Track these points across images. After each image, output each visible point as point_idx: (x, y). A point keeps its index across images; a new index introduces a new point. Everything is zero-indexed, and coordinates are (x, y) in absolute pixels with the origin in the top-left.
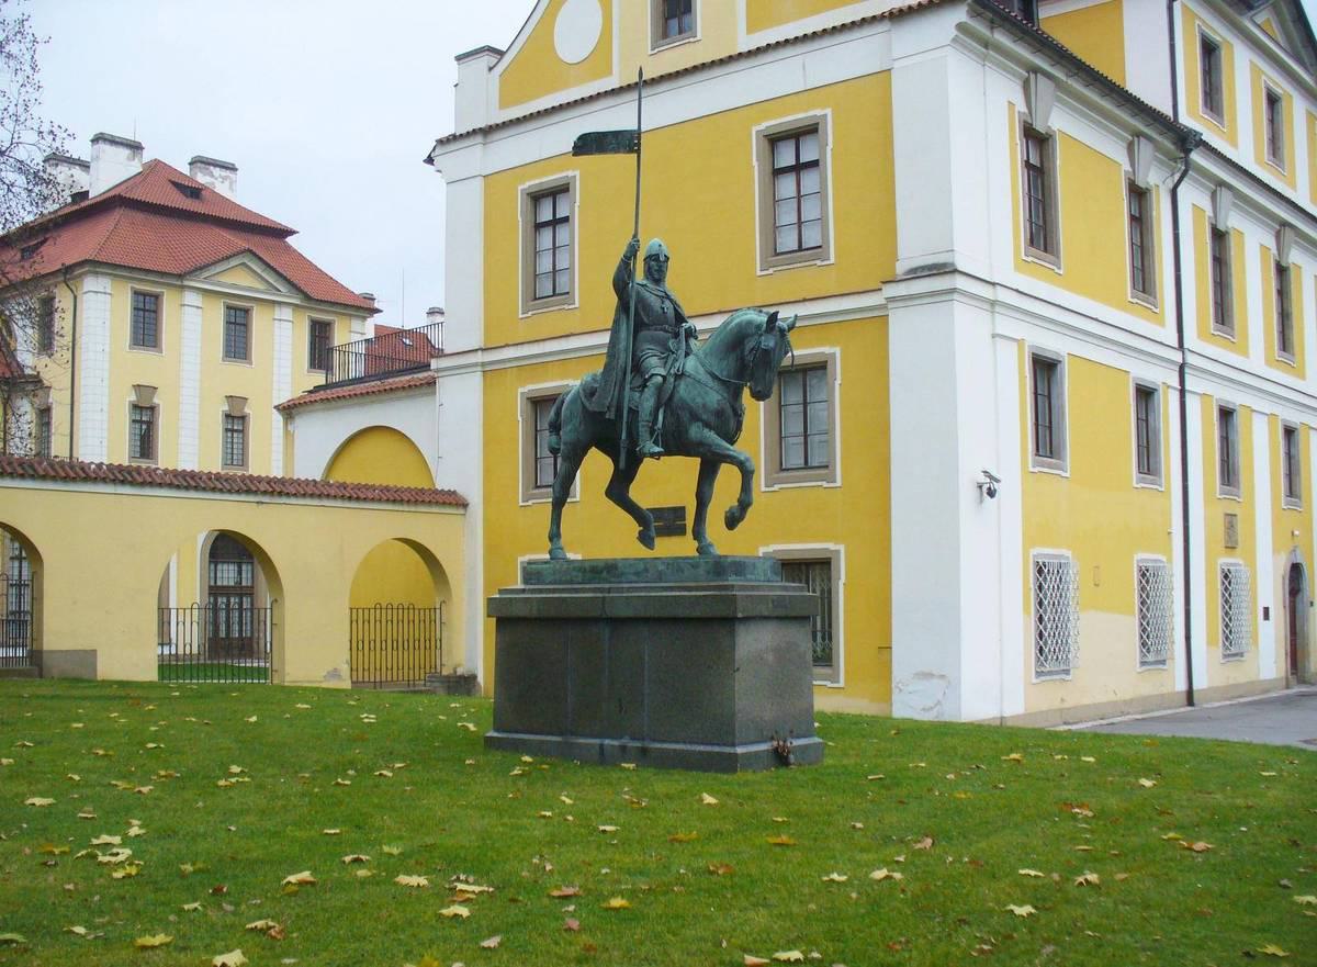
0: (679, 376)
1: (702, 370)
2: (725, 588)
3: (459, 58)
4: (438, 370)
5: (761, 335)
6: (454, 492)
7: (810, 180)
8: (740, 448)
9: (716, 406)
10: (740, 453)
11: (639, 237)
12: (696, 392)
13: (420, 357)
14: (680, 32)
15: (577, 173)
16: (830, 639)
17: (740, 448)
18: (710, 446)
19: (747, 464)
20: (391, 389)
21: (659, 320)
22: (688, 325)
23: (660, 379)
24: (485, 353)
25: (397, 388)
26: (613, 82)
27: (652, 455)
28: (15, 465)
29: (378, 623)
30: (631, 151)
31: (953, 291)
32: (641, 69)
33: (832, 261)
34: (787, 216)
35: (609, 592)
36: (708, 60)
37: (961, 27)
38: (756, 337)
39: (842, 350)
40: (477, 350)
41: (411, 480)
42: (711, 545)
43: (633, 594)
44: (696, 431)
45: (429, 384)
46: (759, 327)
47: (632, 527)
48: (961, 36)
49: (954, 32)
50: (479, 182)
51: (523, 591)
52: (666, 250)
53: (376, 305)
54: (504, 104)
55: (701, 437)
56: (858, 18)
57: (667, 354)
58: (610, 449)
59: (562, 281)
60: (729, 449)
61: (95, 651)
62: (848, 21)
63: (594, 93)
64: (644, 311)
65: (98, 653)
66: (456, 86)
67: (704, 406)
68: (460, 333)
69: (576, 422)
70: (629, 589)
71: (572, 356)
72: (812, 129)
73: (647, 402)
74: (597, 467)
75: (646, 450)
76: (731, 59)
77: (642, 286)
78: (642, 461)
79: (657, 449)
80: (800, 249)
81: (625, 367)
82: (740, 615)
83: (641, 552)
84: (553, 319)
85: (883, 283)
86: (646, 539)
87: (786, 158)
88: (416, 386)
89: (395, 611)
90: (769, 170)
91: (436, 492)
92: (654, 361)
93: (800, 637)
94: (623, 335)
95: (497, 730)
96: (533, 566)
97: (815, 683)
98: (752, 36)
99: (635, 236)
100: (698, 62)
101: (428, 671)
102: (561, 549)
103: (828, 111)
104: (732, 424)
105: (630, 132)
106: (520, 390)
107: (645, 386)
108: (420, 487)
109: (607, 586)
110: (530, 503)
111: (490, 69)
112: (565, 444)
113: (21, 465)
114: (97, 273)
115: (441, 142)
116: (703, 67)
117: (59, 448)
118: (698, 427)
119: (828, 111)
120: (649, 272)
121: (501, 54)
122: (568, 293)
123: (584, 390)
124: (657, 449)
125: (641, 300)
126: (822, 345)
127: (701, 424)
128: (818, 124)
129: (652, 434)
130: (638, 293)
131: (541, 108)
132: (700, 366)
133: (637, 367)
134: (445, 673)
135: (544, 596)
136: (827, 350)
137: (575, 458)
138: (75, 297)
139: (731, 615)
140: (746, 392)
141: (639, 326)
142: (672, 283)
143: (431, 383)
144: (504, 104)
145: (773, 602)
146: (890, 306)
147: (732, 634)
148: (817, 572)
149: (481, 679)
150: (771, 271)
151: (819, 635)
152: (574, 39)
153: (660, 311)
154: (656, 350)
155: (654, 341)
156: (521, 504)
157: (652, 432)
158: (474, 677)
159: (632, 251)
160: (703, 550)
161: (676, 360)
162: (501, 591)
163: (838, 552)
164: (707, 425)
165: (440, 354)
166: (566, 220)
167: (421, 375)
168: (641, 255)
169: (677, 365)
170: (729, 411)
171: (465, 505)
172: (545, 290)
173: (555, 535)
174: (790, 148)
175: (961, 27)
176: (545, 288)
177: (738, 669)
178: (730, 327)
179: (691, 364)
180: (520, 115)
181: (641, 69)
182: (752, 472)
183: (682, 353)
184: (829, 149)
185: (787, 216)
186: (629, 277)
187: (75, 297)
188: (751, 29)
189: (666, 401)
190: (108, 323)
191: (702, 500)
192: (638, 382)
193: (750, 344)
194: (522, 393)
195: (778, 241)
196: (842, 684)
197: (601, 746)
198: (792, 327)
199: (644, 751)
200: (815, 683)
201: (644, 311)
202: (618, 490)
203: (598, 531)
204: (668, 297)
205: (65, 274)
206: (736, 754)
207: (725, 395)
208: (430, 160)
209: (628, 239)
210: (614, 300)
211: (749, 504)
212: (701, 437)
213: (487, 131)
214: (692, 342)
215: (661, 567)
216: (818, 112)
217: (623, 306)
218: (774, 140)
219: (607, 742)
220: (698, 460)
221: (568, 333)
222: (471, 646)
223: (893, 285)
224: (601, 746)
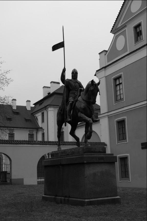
3: (99, 54)
4: (100, 118)
6: (104, 143)
9: (83, 107)
11: (65, 68)
15: (122, 73)
18: (82, 118)
24: (108, 113)
26: (128, 53)
28: (19, 142)
40: (106, 113)
50: (104, 78)
54: (108, 62)
59: (122, 96)
61: (23, 179)
65: (24, 179)
66: (99, 59)
67: (81, 107)
71: (124, 112)
82: (85, 162)
95: (45, 195)
99: (65, 67)
106: (115, 120)
111: (105, 55)
113: (22, 142)
114: (51, 107)
115: (97, 71)
117: (46, 140)
121: (107, 51)
127: (80, 112)
138: (47, 112)
144: (108, 62)
145: (98, 158)
153: (74, 86)
156: (117, 144)
159: (64, 70)
164: (82, 112)
166: (121, 83)
177: (86, 177)
187: (47, 112)
190: (53, 116)
193: (89, 89)
194: (116, 121)
205: (45, 108)
206: (85, 201)
208: (95, 75)
213: (105, 67)
215: (73, 150)
221: (123, 107)
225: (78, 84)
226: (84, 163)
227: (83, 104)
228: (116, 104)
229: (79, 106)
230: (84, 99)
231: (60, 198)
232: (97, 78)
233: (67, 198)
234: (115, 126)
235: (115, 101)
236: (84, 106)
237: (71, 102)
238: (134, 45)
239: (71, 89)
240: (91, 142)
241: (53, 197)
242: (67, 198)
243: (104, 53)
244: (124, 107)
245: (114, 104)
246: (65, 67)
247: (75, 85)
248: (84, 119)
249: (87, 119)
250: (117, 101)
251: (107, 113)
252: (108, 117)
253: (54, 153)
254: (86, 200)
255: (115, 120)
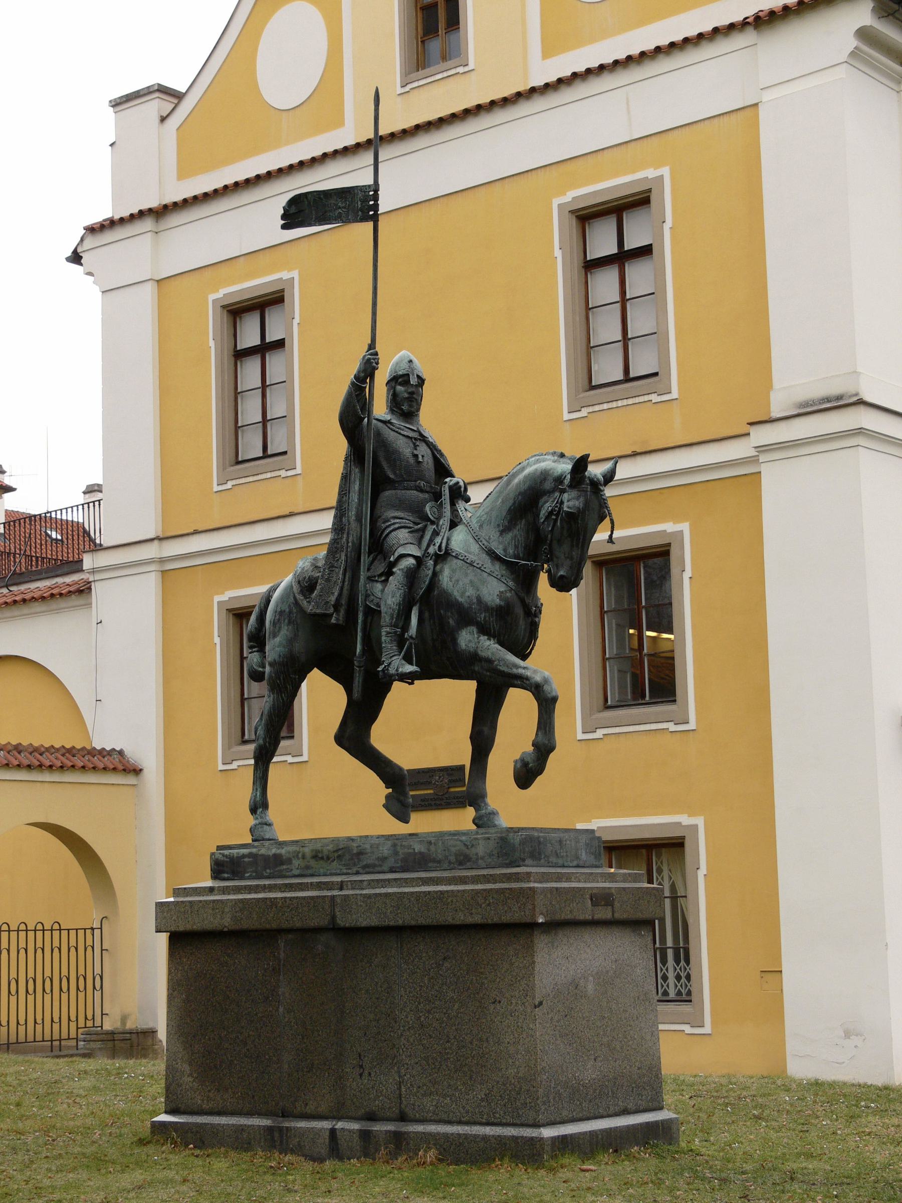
0: (444, 556)
1: (475, 547)
2: (516, 877)
3: (118, 103)
4: (93, 571)
5: (563, 491)
6: (121, 753)
7: (639, 276)
8: (536, 665)
9: (498, 601)
10: (535, 672)
11: (378, 348)
12: (467, 581)
13: (63, 554)
14: (444, 58)
15: (295, 274)
16: (688, 961)
17: (536, 665)
19: (546, 688)
20: (24, 601)
21: (409, 474)
22: (455, 480)
23: (411, 561)
25: (33, 599)
27: (409, 678)
29: (39, 951)
30: (365, 218)
31: (860, 432)
32: (377, 89)
33: (675, 394)
34: (607, 328)
35: (341, 889)
36: (485, 100)
37: (863, 34)
38: (557, 494)
39: (691, 525)
40: (152, 540)
41: (52, 734)
42: (494, 813)
43: (378, 891)
44: (467, 639)
45: (80, 592)
46: (559, 480)
47: (377, 789)
48: (865, 48)
49: (852, 43)
51: (211, 890)
52: (422, 367)
53: (7, 481)
54: (183, 173)
55: (471, 647)
56: (708, 28)
57: (422, 524)
58: (340, 672)
60: (517, 667)
62: (693, 32)
63: (318, 153)
64: (388, 459)
66: (112, 145)
67: (479, 600)
68: (127, 520)
69: (285, 631)
70: (372, 884)
72: (641, 201)
73: (389, 595)
74: (321, 700)
75: (392, 671)
76: (519, 96)
77: (384, 422)
78: (388, 690)
79: (409, 668)
80: (627, 379)
81: (360, 544)
83: (393, 826)
84: (265, 489)
85: (751, 424)
86: (399, 807)
87: (603, 243)
88: (61, 594)
89: (31, 934)
90: (578, 262)
91: (93, 752)
92: (403, 535)
93: (625, 952)
94: (354, 497)
96: (226, 852)
97: (661, 1027)
98: (548, 61)
99: (372, 346)
100: (470, 103)
101: (81, 1023)
102: (270, 825)
103: (665, 171)
104: (522, 624)
105: (363, 189)
106: (217, 599)
107: (389, 573)
108: (68, 747)
109: (338, 879)
110: (234, 765)
111: (163, 119)
112: (270, 664)
115: (91, 230)
116: (479, 109)
118: (472, 633)
119: (665, 171)
120: (395, 403)
121: (178, 96)
122: (285, 453)
123: (299, 582)
124: (409, 668)
125: (382, 443)
126: (663, 520)
127: (474, 629)
128: (650, 190)
129: (400, 646)
130: (378, 434)
131: (241, 177)
132: (472, 540)
133: (378, 545)
134: (107, 1027)
135: (240, 897)
136: (669, 527)
137: (286, 683)
139: (529, 920)
140: (543, 578)
141: (380, 484)
142: (430, 419)
143: (84, 590)
144: (183, 173)
146: (762, 458)
147: (530, 949)
148: (664, 858)
149: (162, 1035)
150: (584, 412)
151: (670, 953)
152: (288, 68)
153: (412, 460)
154: (408, 518)
155: (401, 505)
156: (221, 767)
157: (401, 641)
158: (153, 1032)
159: (368, 370)
160: (483, 821)
161: (436, 533)
162: (177, 892)
163: (695, 828)
164: (484, 630)
165: (97, 548)
167: (68, 579)
168: (382, 377)
169: (438, 540)
170: (519, 611)
171: (137, 771)
172: (251, 446)
173: (259, 806)
174: (611, 231)
175: (863, 34)
176: (251, 445)
177: (541, 1003)
178: (516, 481)
179: (459, 539)
180: (209, 188)
181: (377, 89)
182: (555, 700)
183: (445, 522)
184: (667, 226)
185: (607, 328)
186: (363, 408)
188: (548, 52)
189: (424, 594)
191: (482, 741)
192: (380, 568)
193: (547, 506)
195: (595, 368)
196: (707, 1029)
197: (333, 1131)
198: (609, 477)
199: (398, 1138)
200: (661, 1027)
201: (388, 459)
202: (354, 735)
203: (326, 797)
204: (423, 439)
207: (511, 583)
208: (76, 258)
209: (361, 351)
210: (341, 445)
211: (551, 749)
212: (471, 647)
213: (161, 212)
214: (461, 505)
215: (418, 847)
216: (651, 173)
217: (356, 455)
218: (585, 217)
219: (340, 1125)
220: (472, 685)
222: (142, 985)
223: (768, 427)
224: (333, 1131)
225: (429, 451)
226: (531, 927)
227: (495, 582)
228: (229, 485)
229: (470, 592)
230: (499, 552)
231: (326, 1125)
232: (91, 278)
233: (390, 1127)
234: (217, 640)
235: (222, 468)
236: (501, 592)
237: (411, 561)
238: (400, 90)
239: (392, 476)
240: (36, 744)
241: (266, 1122)
242: (390, 1127)
243: (155, 106)
244: (291, 515)
245: (216, 488)
246: (372, 346)
247: (416, 456)
248: (502, 668)
249: (521, 671)
250: (238, 463)
251: (156, 542)
252: (164, 572)
253: (244, 856)
254: (548, 1133)
255: (217, 599)
